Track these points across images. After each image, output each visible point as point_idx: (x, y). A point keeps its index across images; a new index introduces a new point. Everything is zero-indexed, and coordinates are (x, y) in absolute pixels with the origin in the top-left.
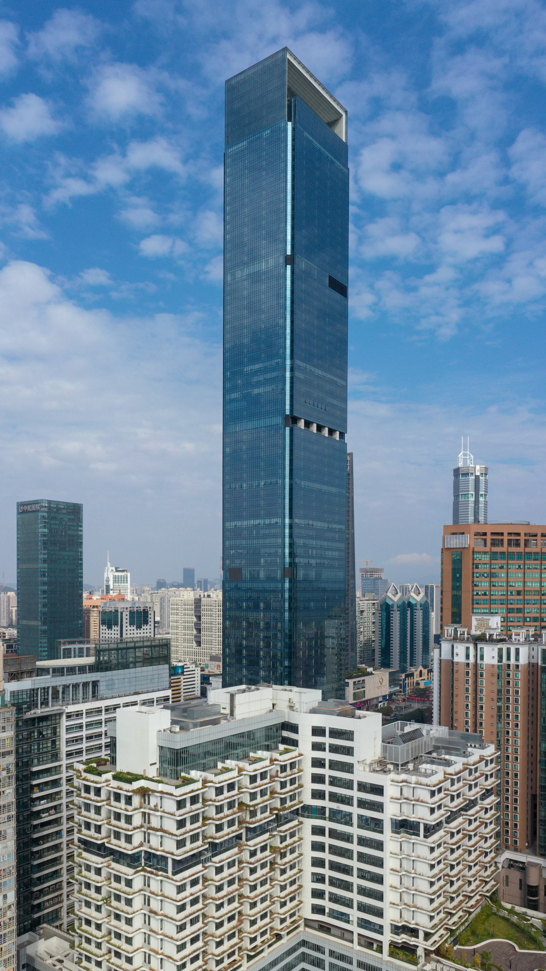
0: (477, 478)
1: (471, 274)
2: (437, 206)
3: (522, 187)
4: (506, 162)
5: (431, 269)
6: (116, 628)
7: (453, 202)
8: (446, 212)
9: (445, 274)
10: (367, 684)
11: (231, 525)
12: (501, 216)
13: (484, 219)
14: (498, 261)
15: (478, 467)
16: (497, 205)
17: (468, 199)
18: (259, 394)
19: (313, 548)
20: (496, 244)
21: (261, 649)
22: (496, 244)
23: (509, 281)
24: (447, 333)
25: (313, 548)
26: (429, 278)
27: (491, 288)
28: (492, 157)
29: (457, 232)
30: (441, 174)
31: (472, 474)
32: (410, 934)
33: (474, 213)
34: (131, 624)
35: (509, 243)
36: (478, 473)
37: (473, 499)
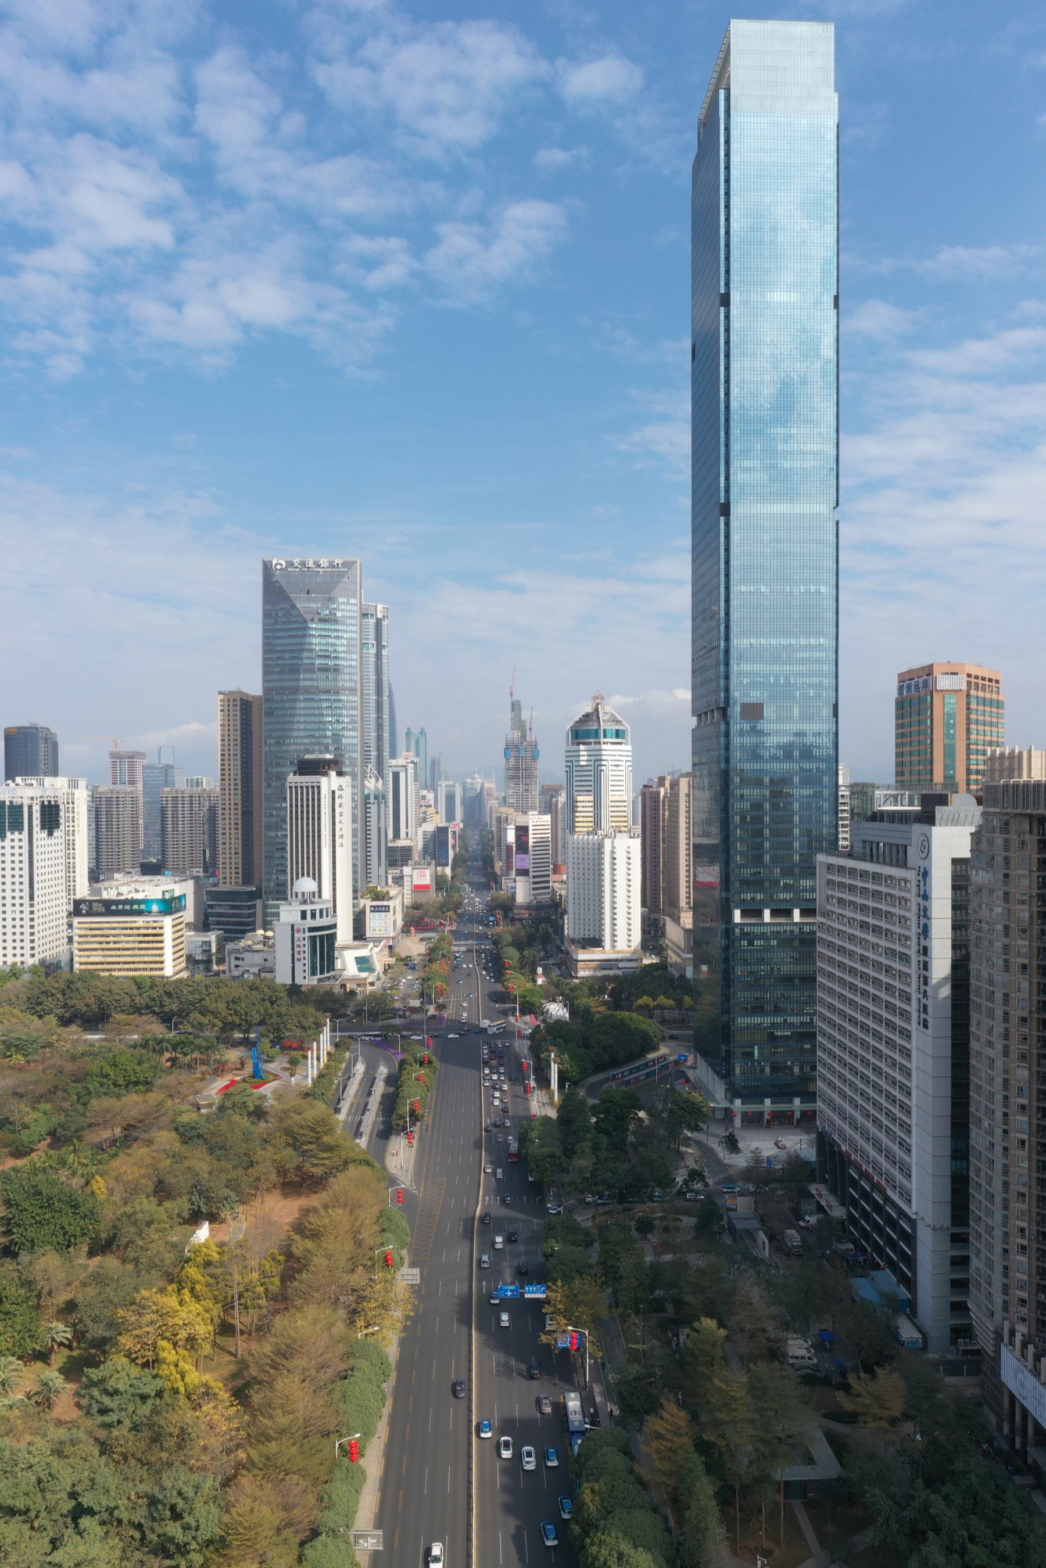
1: (114, 276)
2: (71, 125)
4: (188, 94)
5: (44, 240)
7: (96, 131)
8: (80, 146)
9: (68, 258)
10: (282, 908)
11: (267, 656)
12: (173, 187)
13: (144, 184)
14: (164, 264)
15: (380, 607)
16: (173, 167)
17: (128, 138)
18: (792, 469)
20: (161, 234)
21: (768, 826)
22: (161, 234)
23: (178, 305)
24: (64, 367)
26: (43, 257)
27: (149, 311)
28: (166, 73)
30: (77, 66)
31: (372, 615)
33: (133, 166)
36: (380, 616)
37: (374, 651)
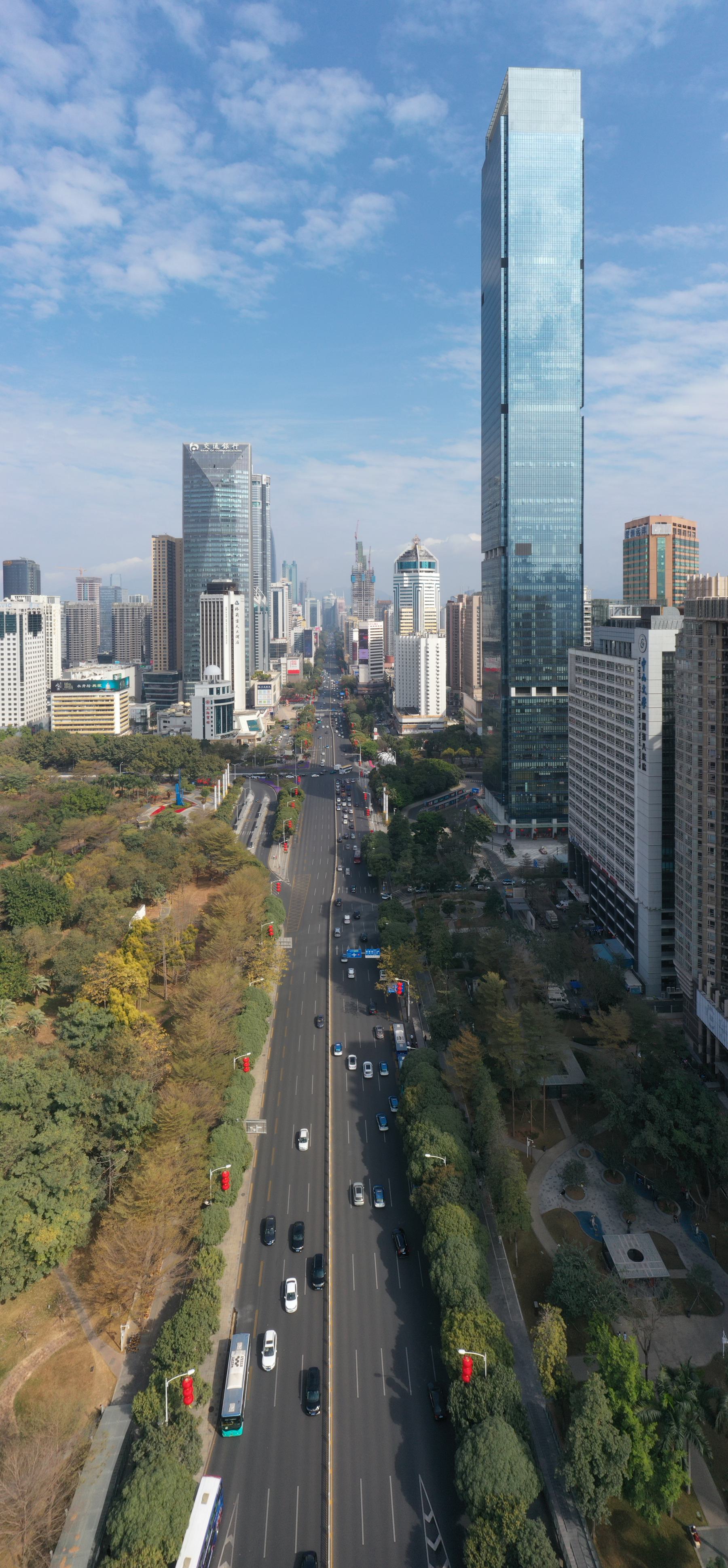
0: (263, 488)
1: (79, 246)
2: (49, 141)
3: (145, 156)
5: (31, 221)
6: (11, 636)
7: (67, 145)
8: (56, 156)
12: (120, 184)
14: (114, 238)
15: (264, 477)
19: (554, 524)
20: (112, 216)
23: (124, 266)
24: (45, 310)
25: (554, 524)
26: (30, 233)
27: (104, 270)
28: (116, 105)
29: (69, 185)
32: (235, 1091)
33: (92, 169)
34: (30, 630)
35: (126, 219)
36: (264, 483)
